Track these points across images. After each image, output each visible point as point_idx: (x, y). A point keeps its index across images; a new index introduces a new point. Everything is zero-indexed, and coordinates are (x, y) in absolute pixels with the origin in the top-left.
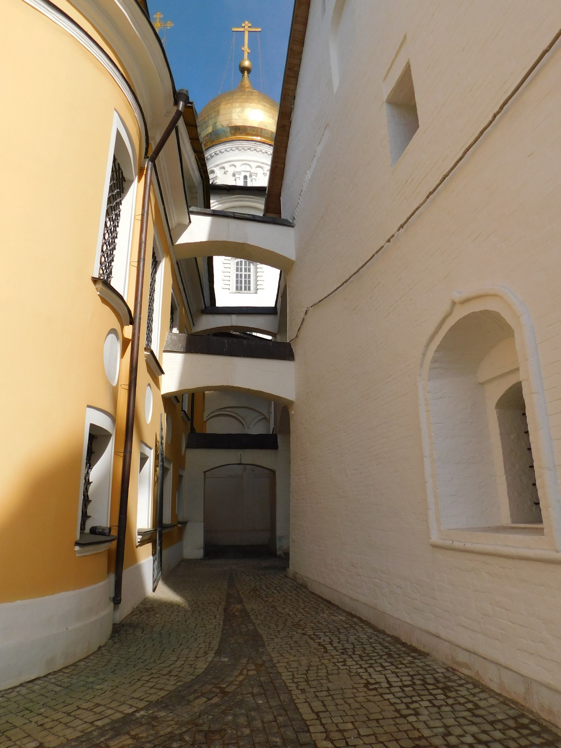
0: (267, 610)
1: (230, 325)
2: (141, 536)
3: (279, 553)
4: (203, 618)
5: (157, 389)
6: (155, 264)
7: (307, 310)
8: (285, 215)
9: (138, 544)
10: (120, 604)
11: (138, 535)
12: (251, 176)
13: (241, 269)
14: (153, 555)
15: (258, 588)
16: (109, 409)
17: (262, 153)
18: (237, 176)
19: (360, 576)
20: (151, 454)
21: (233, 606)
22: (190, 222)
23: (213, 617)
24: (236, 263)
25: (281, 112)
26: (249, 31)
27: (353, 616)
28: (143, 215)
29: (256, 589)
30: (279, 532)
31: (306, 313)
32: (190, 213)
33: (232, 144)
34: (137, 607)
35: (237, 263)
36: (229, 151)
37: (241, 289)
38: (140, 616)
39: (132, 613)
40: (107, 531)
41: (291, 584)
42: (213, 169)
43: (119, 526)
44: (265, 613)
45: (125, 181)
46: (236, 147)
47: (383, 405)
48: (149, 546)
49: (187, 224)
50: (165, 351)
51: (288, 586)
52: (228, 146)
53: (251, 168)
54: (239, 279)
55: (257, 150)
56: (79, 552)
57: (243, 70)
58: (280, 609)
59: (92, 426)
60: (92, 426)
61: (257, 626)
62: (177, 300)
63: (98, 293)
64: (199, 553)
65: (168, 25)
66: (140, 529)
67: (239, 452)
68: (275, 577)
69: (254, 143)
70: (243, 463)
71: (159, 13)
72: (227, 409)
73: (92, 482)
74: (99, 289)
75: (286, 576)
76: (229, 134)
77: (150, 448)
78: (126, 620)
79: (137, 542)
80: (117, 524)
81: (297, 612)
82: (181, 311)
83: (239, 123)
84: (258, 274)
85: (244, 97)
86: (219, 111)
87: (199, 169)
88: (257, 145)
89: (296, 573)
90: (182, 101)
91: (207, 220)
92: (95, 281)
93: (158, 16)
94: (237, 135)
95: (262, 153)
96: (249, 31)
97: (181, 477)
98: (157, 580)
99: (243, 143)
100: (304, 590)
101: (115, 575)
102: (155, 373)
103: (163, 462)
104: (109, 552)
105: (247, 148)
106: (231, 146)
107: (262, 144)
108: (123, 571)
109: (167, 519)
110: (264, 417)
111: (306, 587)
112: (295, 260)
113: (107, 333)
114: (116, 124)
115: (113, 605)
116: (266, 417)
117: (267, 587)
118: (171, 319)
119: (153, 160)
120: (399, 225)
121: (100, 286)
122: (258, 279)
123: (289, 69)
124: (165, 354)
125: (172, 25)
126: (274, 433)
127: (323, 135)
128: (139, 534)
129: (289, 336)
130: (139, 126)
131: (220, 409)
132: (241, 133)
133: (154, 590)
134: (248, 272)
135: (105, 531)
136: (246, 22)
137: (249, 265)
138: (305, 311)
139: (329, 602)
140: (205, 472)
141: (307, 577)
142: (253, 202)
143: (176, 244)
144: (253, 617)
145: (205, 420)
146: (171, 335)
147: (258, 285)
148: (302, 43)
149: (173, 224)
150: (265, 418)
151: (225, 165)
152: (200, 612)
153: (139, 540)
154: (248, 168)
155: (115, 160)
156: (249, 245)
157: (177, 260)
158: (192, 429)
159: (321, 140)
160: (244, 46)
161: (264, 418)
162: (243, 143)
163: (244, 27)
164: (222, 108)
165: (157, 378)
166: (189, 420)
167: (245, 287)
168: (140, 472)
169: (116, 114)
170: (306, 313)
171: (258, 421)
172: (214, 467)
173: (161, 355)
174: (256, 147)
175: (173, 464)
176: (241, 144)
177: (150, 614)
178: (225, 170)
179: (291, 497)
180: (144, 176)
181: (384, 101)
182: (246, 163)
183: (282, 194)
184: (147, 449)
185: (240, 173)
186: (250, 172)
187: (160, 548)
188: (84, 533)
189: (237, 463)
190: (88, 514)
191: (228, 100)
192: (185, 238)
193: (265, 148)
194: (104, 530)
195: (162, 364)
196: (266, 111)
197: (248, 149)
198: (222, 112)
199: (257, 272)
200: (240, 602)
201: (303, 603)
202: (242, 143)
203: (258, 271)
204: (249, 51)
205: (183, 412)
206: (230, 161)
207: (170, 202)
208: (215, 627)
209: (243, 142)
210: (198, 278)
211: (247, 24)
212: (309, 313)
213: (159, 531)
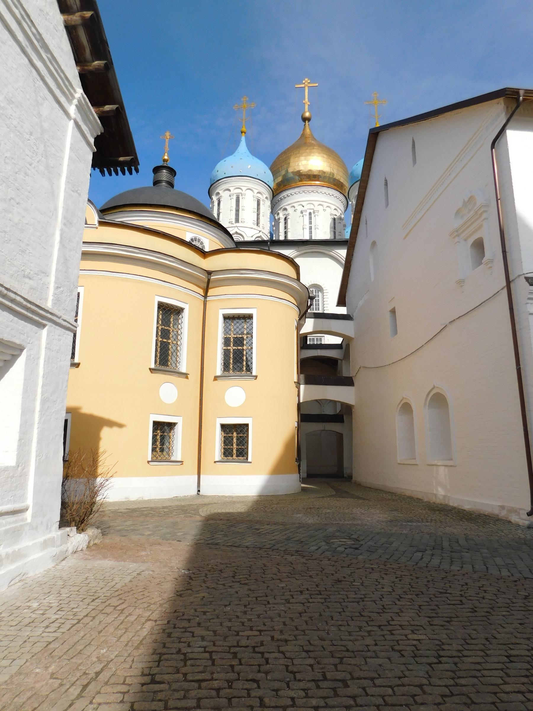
3: (345, 476)
12: (314, 212)
18: (304, 213)
30: (345, 465)
42: (286, 207)
52: (296, 190)
55: (319, 192)
57: (305, 119)
65: (252, 106)
67: (324, 424)
86: (289, 163)
136: (306, 79)
137: (318, 293)
142: (319, 249)
151: (295, 205)
154: (312, 207)
160: (304, 99)
167: (316, 308)
182: (310, 202)
185: (306, 211)
198: (291, 164)
206: (298, 202)
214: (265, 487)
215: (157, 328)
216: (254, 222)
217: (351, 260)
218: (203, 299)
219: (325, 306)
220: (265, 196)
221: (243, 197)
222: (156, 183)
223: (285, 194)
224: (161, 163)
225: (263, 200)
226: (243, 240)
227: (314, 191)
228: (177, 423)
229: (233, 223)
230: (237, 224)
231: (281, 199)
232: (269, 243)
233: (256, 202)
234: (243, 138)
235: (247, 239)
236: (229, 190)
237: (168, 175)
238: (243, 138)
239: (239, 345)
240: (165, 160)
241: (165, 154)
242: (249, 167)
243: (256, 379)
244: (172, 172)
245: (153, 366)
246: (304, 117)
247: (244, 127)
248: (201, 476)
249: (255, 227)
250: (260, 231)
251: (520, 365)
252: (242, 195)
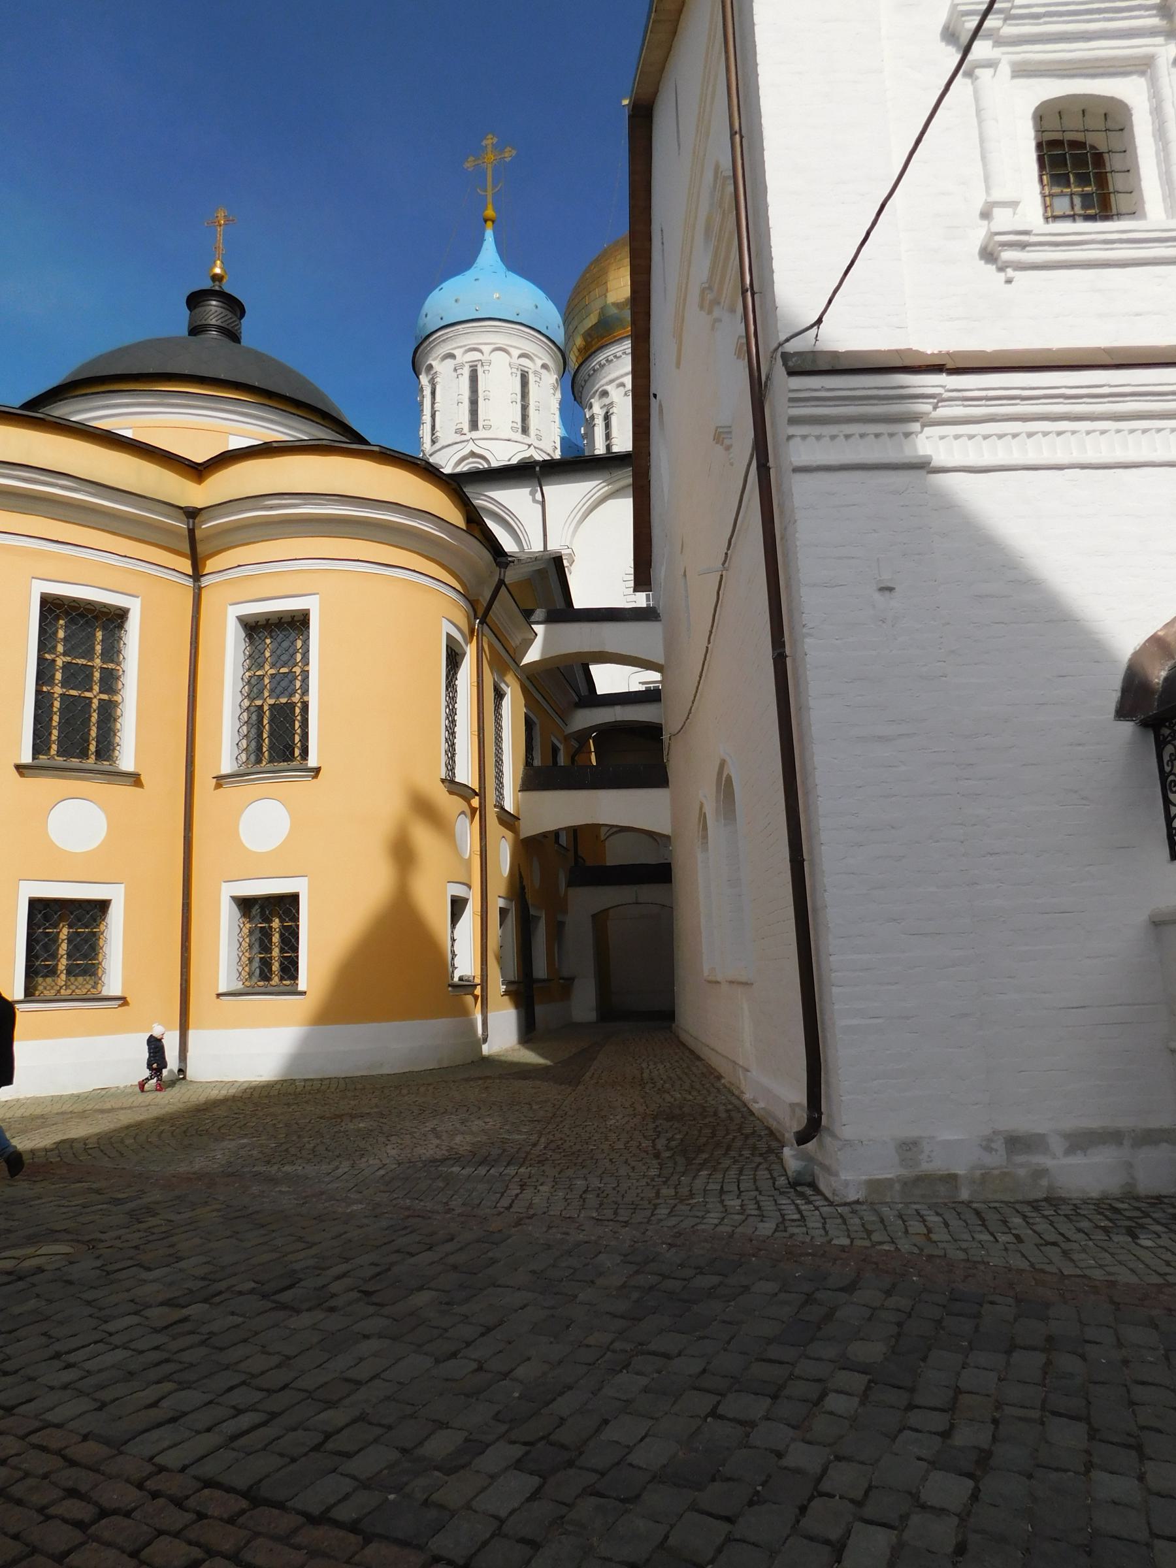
6: (499, 695)
40: (471, 979)
43: (482, 975)
64: (592, 1016)
65: (506, 155)
67: (635, 888)
71: (490, 136)
92: (443, 781)
93: (489, 142)
97: (561, 925)
109: (540, 969)
114: (448, 628)
125: (514, 153)
164: (611, 278)
180: (475, 638)
198: (610, 285)
214: (298, 1058)
215: (305, 692)
216: (515, 425)
218: (189, 582)
220: (539, 363)
221: (486, 368)
222: (196, 330)
223: (601, 357)
224: (207, 285)
225: (535, 372)
226: (486, 466)
229: (464, 431)
230: (475, 434)
231: (594, 371)
232: (538, 469)
233: (519, 378)
234: (489, 236)
235: (495, 464)
236: (452, 356)
237: (225, 312)
238: (489, 236)
239: (90, 676)
240: (216, 278)
241: (215, 262)
242: (496, 295)
243: (316, 777)
244: (235, 306)
245: (26, 758)
247: (490, 206)
248: (192, 1034)
249: (518, 436)
250: (530, 446)
251: (783, 645)
252: (482, 365)
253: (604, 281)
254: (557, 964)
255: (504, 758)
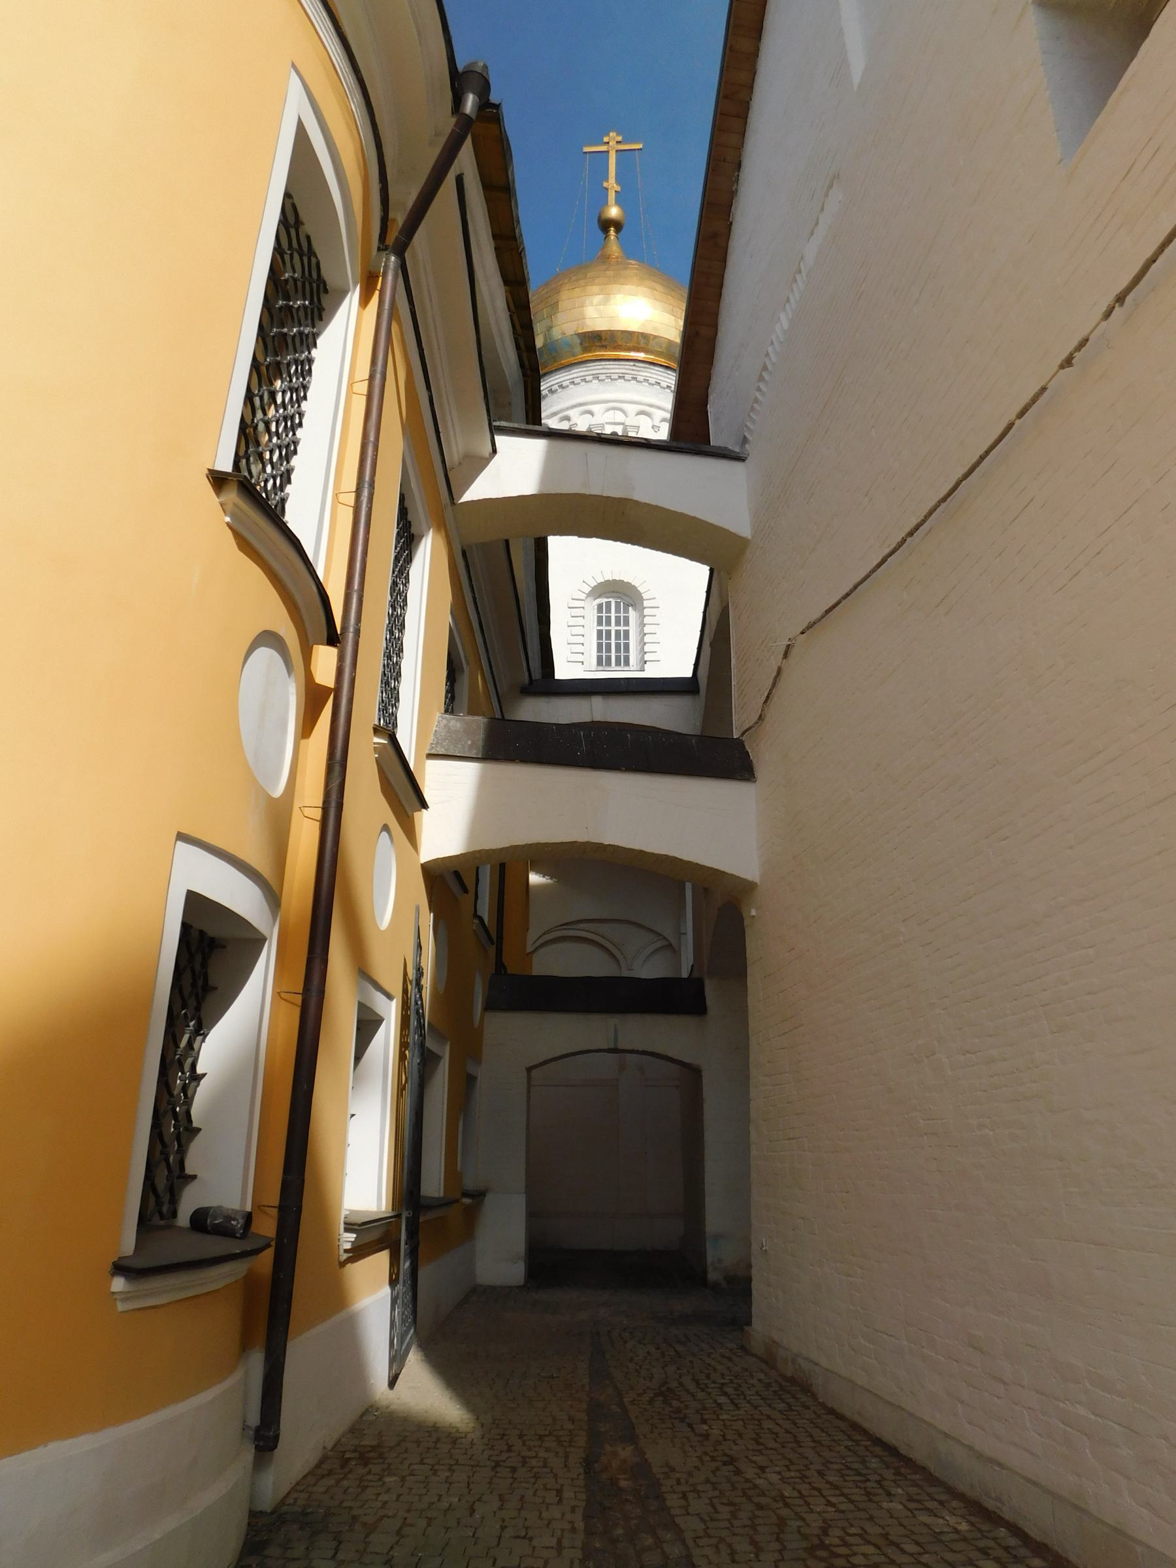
0: (713, 1472)
1: (587, 719)
2: (355, 1236)
3: (713, 1276)
4: (523, 1496)
5: (410, 846)
6: (407, 541)
7: (788, 646)
8: (717, 439)
9: (344, 1256)
10: (276, 1450)
11: (347, 1230)
13: (609, 619)
14: (393, 1282)
15: (674, 1385)
16: (256, 855)
17: (650, 384)
19: (1004, 1383)
20: (391, 1012)
21: (608, 1448)
22: (494, 451)
23: (551, 1497)
24: (596, 607)
25: (708, 203)
26: (617, 151)
27: (994, 1518)
28: (372, 378)
29: (669, 1389)
31: (786, 655)
32: (494, 430)
33: (585, 369)
34: (335, 1445)
35: (600, 607)
36: (579, 384)
37: (609, 663)
38: (338, 1482)
39: (319, 1471)
40: (238, 1224)
41: (762, 1376)
44: (709, 1486)
45: (326, 291)
46: (593, 375)
47: (1071, 848)
48: (382, 1259)
49: (488, 456)
50: (431, 756)
51: (754, 1382)
52: (576, 373)
53: (626, 416)
54: (604, 641)
56: (126, 1297)
57: (606, 225)
58: (750, 1473)
59: (194, 901)
60: (194, 901)
61: (690, 1543)
62: (462, 644)
63: (228, 519)
64: (514, 1272)
66: (352, 1212)
67: (613, 1021)
68: (714, 1348)
69: (632, 364)
70: (621, 1046)
72: (582, 926)
73: (204, 1075)
74: (229, 507)
75: (743, 1348)
76: (578, 349)
77: (390, 997)
78: (295, 1495)
79: (342, 1252)
80: (275, 1201)
81: (804, 1488)
82: (474, 680)
83: (601, 325)
84: (646, 630)
85: (609, 273)
86: (557, 303)
87: (515, 338)
88: (638, 369)
89: (774, 1342)
90: (474, 93)
91: (535, 448)
92: (218, 480)
94: (595, 351)
95: (650, 384)
96: (617, 151)
97: (471, 1080)
98: (398, 1357)
99: (608, 367)
100: (804, 1399)
101: (264, 1354)
102: (404, 803)
103: (422, 1036)
104: (250, 1282)
105: (616, 376)
106: (582, 374)
107: (647, 366)
108: (289, 1345)
109: (433, 1184)
110: (664, 943)
111: (807, 1389)
112: (749, 537)
113: (250, 641)
114: (295, 106)
115: (253, 1451)
116: (671, 945)
117: (698, 1384)
118: (447, 692)
119: (400, 249)
120: (1110, 298)
121: (232, 495)
122: (647, 639)
123: (726, 97)
124: (431, 764)
126: (696, 975)
127: (822, 209)
128: (349, 1227)
129: (740, 721)
130: (360, 138)
131: (562, 925)
132: (604, 347)
133: (392, 1383)
134: (624, 626)
135: (234, 1223)
136: (611, 134)
137: (626, 611)
138: (783, 649)
139: (892, 1450)
140: (529, 1070)
141: (807, 1359)
143: (461, 501)
144: (673, 1501)
145: (529, 949)
146: (446, 718)
147: (645, 653)
148: (757, 31)
149: (454, 453)
150: (670, 946)
151: (571, 413)
152: (514, 1470)
153: (348, 1246)
154: (619, 417)
155: (287, 195)
156: (637, 502)
157: (462, 547)
158: (500, 966)
159: (817, 223)
160: (607, 179)
161: (666, 946)
162: (608, 367)
163: (608, 143)
164: (564, 298)
165: (408, 817)
166: (493, 944)
168: (358, 1058)
169: (295, 80)
170: (786, 655)
171: (649, 956)
172: (551, 1057)
173: (422, 768)
174: (636, 373)
175: (451, 1044)
176: (604, 369)
177: (369, 1472)
178: (571, 423)
179: (753, 1134)
180: (377, 293)
181: (1027, 3)
183: (711, 398)
184: (379, 998)
186: (623, 424)
187: (411, 1264)
188: (176, 1226)
189: (606, 1048)
190: (189, 1171)
191: (577, 280)
192: (481, 489)
193: (656, 374)
194: (228, 1218)
195: (424, 788)
196: (655, 299)
197: (620, 377)
198: (562, 305)
199: (645, 625)
200: (630, 1437)
201: (813, 1448)
202: (605, 367)
203: (645, 622)
204: (618, 188)
205: (476, 921)
206: (581, 405)
207: (447, 396)
208: (559, 1541)
209: (607, 363)
210: (514, 602)
211: (613, 137)
212: (794, 652)
213: (407, 1218)
217: (732, 194)
219: (647, 629)
227: (627, 377)
228: (200, 1129)
246: (603, 218)
253: (555, 300)
254: (459, 1164)
255: (405, 665)
